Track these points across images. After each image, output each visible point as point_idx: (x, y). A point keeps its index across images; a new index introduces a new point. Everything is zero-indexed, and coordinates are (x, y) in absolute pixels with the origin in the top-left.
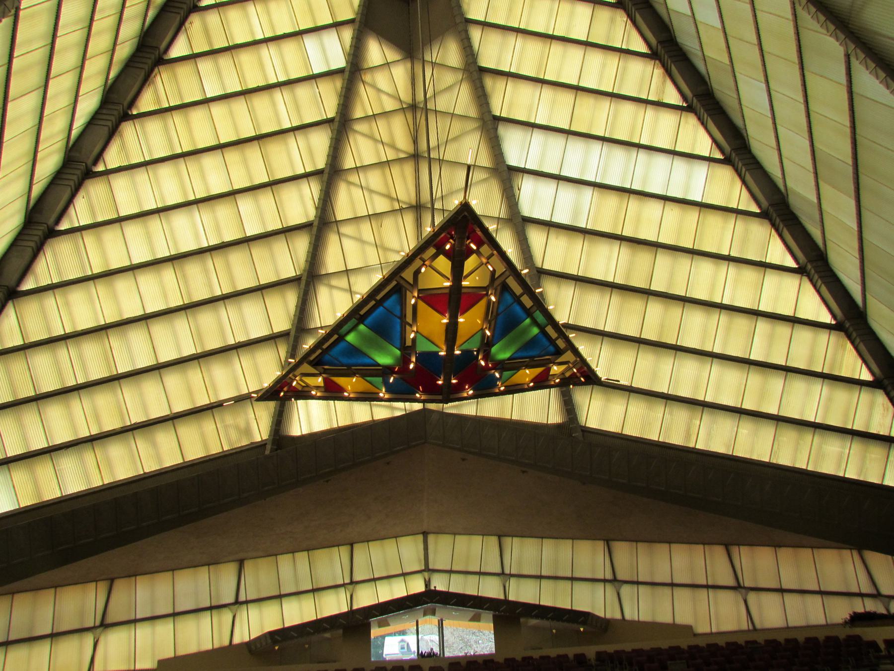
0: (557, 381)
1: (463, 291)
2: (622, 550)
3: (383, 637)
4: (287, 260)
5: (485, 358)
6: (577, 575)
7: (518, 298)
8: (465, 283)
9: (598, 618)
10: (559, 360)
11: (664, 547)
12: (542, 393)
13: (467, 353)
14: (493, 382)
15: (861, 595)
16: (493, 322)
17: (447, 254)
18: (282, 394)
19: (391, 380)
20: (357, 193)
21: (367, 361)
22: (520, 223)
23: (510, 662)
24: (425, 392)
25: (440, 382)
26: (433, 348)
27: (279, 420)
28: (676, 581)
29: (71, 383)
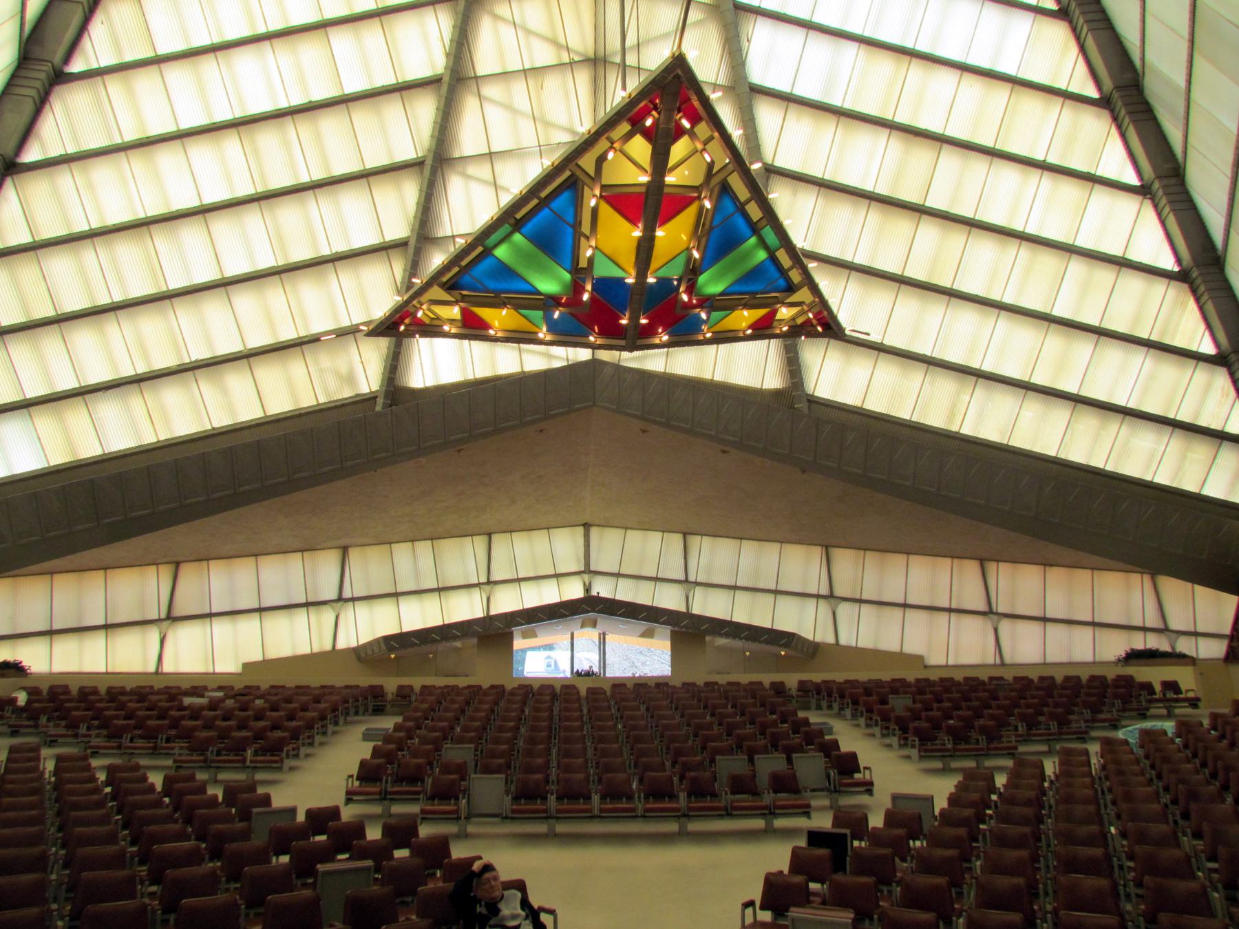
0: (785, 329)
1: (666, 190)
2: (844, 560)
3: (524, 651)
4: (404, 132)
5: (691, 290)
6: (783, 587)
7: (739, 206)
8: (670, 179)
9: (805, 640)
10: (789, 300)
11: (901, 558)
12: (762, 344)
13: (664, 282)
14: (696, 325)
15: (1144, 629)
16: (704, 240)
17: (648, 134)
18: (402, 328)
19: (556, 315)
20: (507, 32)
21: (524, 287)
22: (748, 94)
23: (688, 686)
24: (602, 333)
25: (624, 322)
26: (617, 273)
27: (394, 365)
28: (910, 601)
29: (104, 300)
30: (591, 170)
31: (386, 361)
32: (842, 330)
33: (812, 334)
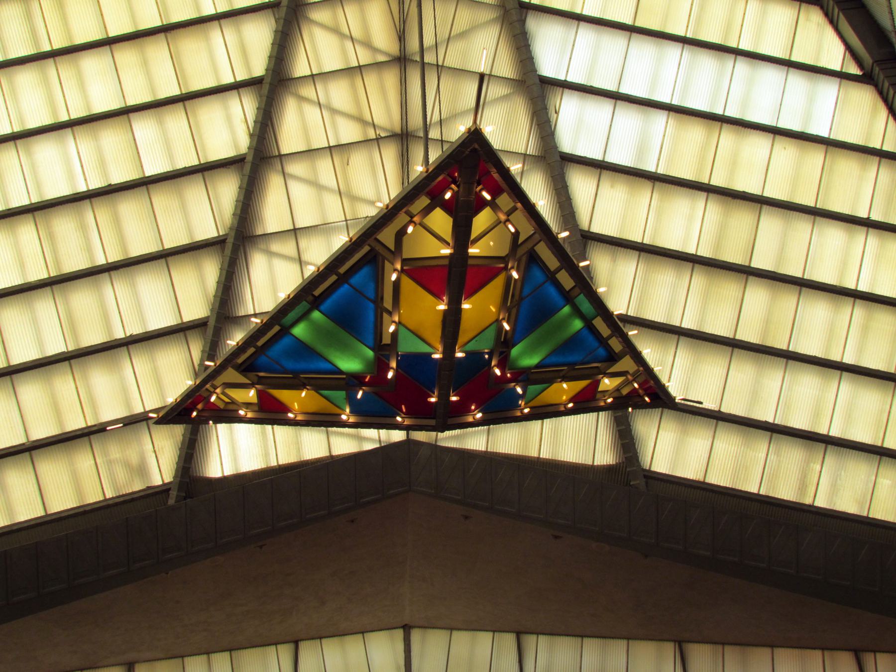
1: (470, 262)
4: (205, 213)
5: (502, 365)
7: (553, 275)
8: (473, 251)
10: (611, 370)
12: (591, 417)
13: (474, 357)
16: (514, 311)
17: (448, 207)
19: (360, 395)
20: (313, 114)
22: (557, 163)
24: (409, 414)
25: (433, 400)
26: (424, 348)
27: (190, 453)
30: (391, 244)
31: (181, 449)
32: (671, 399)
33: (641, 406)
